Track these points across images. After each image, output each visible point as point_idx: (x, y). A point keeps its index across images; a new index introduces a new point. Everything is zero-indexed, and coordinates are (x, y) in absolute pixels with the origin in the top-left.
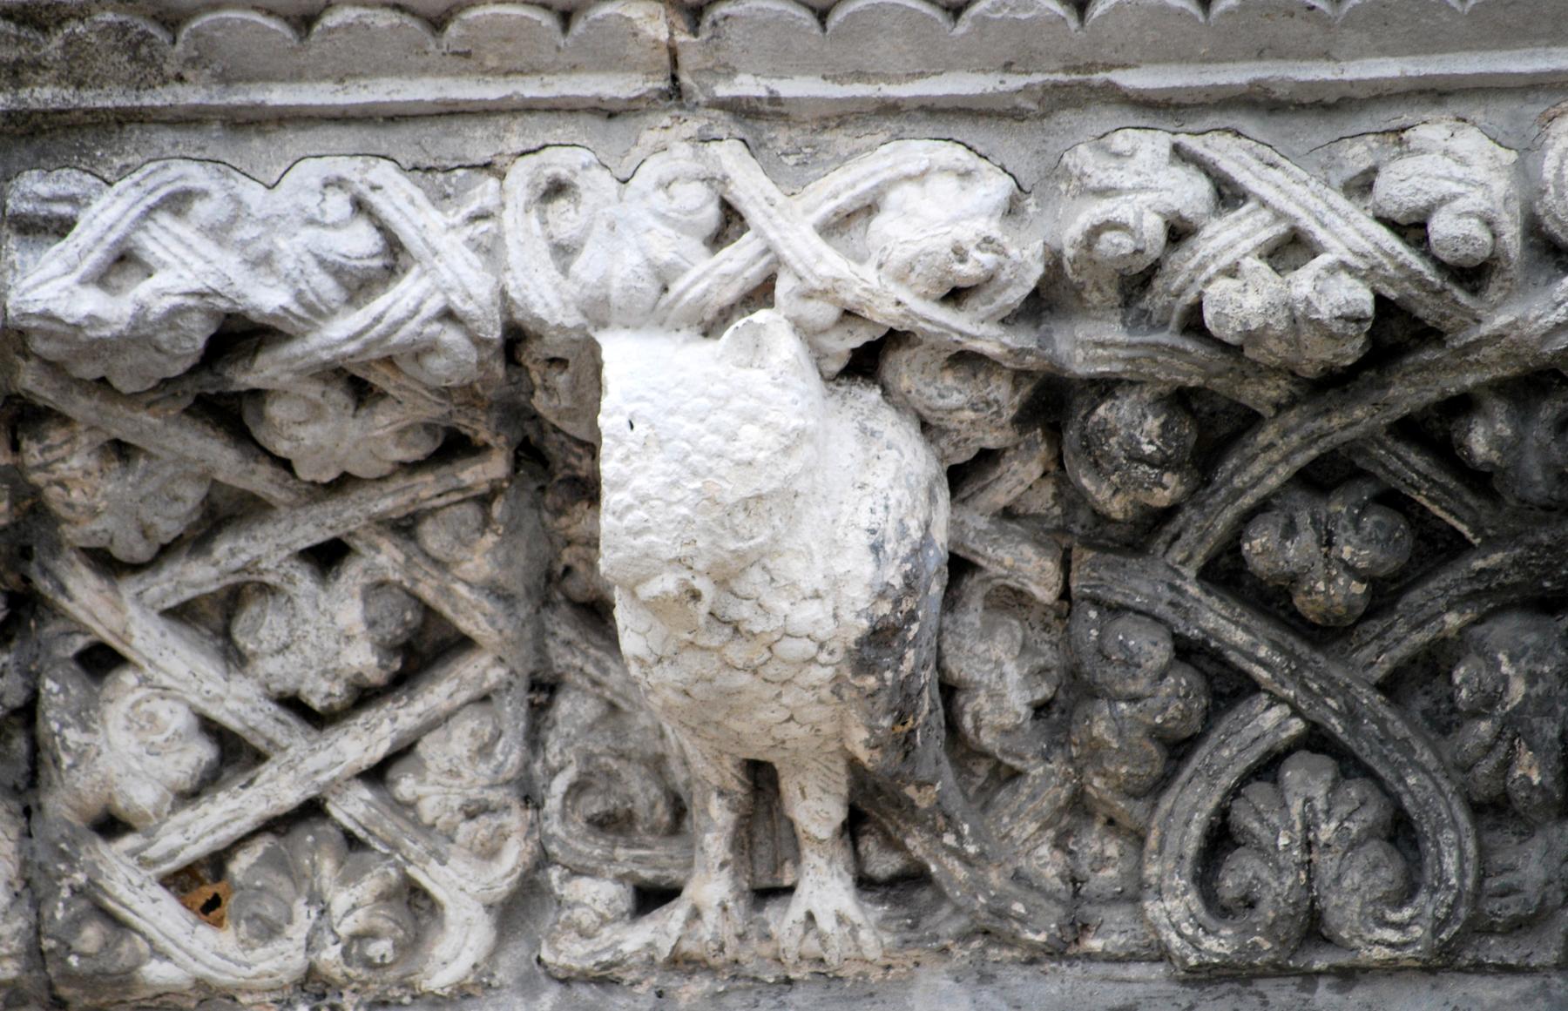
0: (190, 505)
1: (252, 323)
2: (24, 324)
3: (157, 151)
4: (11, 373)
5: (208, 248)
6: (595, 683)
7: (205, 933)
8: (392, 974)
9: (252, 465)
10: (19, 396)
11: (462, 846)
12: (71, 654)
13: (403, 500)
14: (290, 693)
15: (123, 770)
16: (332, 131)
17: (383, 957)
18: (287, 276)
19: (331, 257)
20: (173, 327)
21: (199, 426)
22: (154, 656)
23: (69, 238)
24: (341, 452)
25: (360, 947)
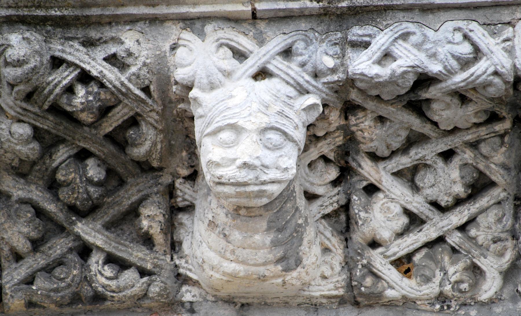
0: (403, 138)
1: (429, 76)
2: (354, 77)
3: (398, 19)
4: (348, 94)
5: (415, 51)
7: (406, 280)
8: (468, 295)
9: (424, 124)
10: (349, 101)
11: (491, 252)
12: (361, 187)
13: (475, 136)
14: (434, 201)
15: (379, 226)
16: (456, 12)
17: (465, 289)
18: (441, 60)
19: (456, 54)
20: (403, 78)
21: (408, 111)
22: (389, 188)
23: (369, 48)
24: (455, 120)
25: (457, 285)
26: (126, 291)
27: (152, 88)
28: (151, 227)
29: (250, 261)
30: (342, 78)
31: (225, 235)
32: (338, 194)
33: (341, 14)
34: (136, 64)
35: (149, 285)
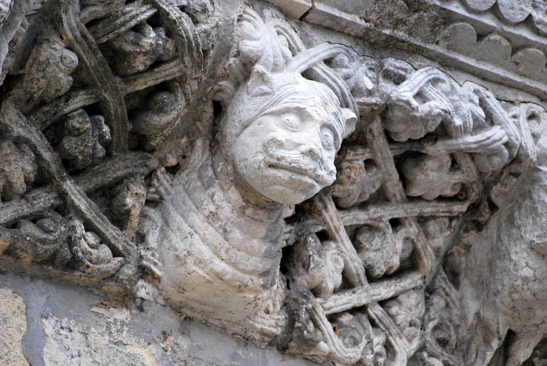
6: (447, 294)
13: (434, 210)
19: (476, 114)
26: (102, 265)
27: (212, 52)
28: (134, 206)
29: (240, 265)
30: (380, 102)
31: (225, 231)
32: (290, 232)
33: (373, 43)
34: (207, 23)
35: (122, 266)
